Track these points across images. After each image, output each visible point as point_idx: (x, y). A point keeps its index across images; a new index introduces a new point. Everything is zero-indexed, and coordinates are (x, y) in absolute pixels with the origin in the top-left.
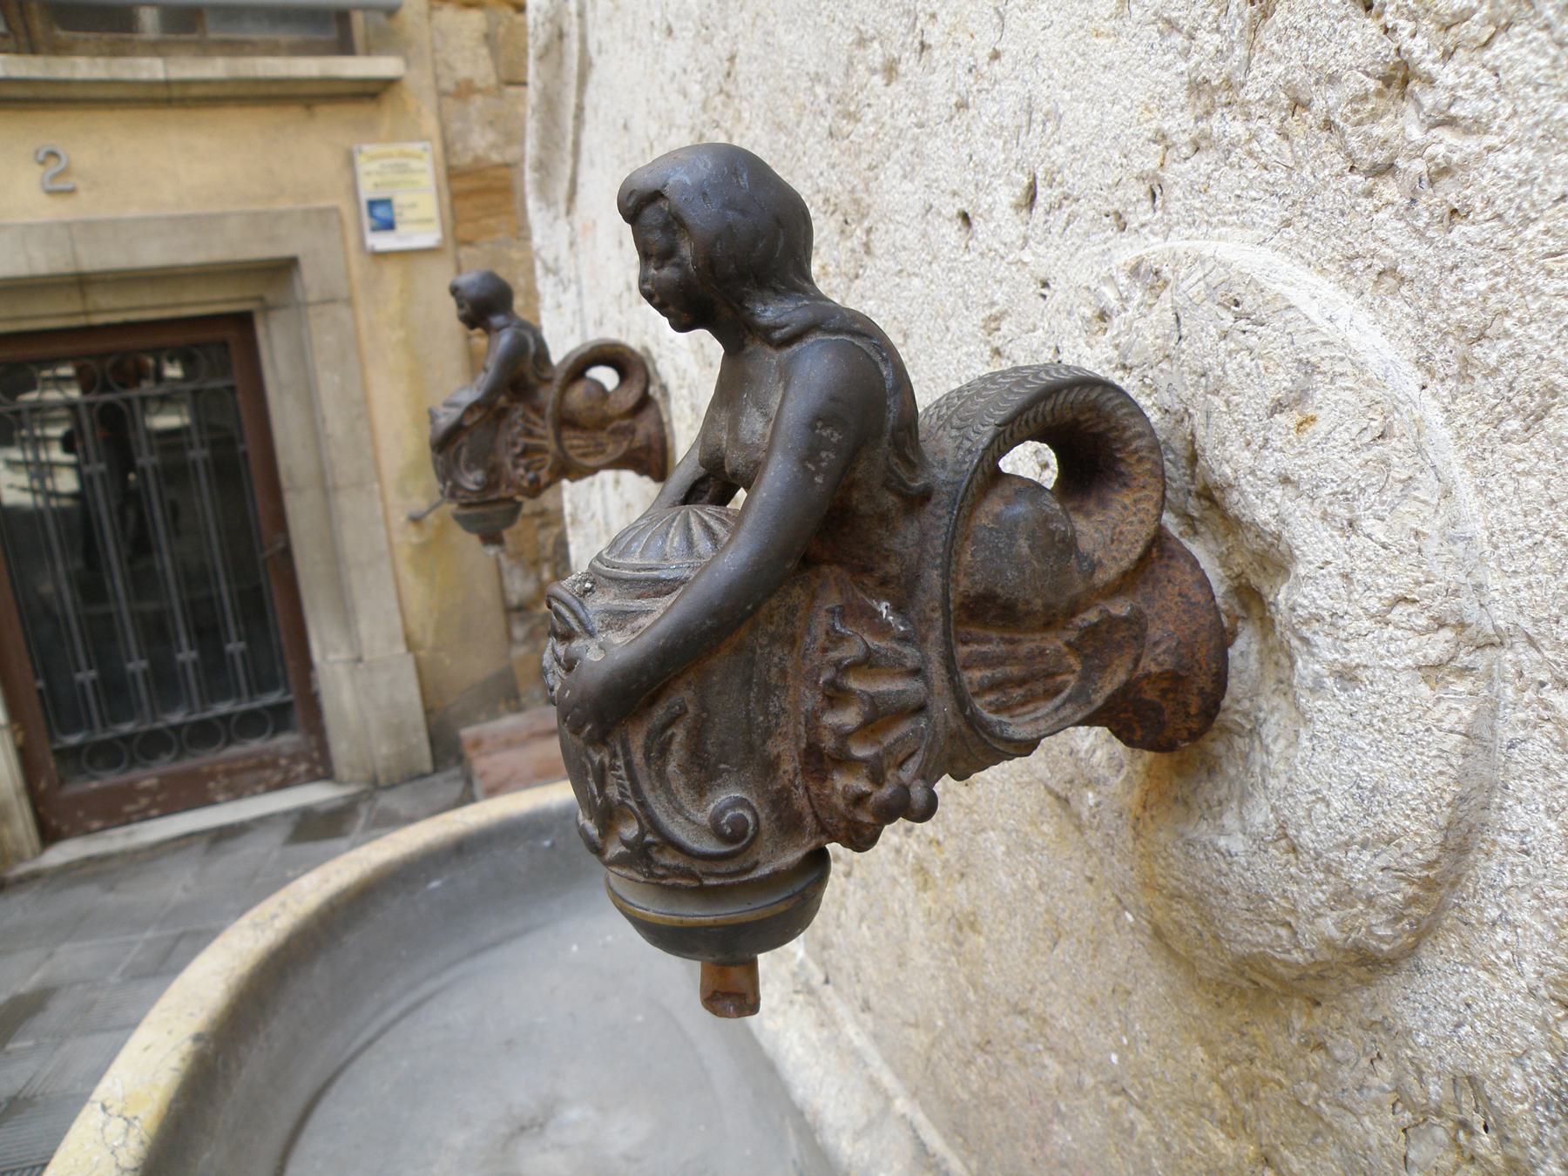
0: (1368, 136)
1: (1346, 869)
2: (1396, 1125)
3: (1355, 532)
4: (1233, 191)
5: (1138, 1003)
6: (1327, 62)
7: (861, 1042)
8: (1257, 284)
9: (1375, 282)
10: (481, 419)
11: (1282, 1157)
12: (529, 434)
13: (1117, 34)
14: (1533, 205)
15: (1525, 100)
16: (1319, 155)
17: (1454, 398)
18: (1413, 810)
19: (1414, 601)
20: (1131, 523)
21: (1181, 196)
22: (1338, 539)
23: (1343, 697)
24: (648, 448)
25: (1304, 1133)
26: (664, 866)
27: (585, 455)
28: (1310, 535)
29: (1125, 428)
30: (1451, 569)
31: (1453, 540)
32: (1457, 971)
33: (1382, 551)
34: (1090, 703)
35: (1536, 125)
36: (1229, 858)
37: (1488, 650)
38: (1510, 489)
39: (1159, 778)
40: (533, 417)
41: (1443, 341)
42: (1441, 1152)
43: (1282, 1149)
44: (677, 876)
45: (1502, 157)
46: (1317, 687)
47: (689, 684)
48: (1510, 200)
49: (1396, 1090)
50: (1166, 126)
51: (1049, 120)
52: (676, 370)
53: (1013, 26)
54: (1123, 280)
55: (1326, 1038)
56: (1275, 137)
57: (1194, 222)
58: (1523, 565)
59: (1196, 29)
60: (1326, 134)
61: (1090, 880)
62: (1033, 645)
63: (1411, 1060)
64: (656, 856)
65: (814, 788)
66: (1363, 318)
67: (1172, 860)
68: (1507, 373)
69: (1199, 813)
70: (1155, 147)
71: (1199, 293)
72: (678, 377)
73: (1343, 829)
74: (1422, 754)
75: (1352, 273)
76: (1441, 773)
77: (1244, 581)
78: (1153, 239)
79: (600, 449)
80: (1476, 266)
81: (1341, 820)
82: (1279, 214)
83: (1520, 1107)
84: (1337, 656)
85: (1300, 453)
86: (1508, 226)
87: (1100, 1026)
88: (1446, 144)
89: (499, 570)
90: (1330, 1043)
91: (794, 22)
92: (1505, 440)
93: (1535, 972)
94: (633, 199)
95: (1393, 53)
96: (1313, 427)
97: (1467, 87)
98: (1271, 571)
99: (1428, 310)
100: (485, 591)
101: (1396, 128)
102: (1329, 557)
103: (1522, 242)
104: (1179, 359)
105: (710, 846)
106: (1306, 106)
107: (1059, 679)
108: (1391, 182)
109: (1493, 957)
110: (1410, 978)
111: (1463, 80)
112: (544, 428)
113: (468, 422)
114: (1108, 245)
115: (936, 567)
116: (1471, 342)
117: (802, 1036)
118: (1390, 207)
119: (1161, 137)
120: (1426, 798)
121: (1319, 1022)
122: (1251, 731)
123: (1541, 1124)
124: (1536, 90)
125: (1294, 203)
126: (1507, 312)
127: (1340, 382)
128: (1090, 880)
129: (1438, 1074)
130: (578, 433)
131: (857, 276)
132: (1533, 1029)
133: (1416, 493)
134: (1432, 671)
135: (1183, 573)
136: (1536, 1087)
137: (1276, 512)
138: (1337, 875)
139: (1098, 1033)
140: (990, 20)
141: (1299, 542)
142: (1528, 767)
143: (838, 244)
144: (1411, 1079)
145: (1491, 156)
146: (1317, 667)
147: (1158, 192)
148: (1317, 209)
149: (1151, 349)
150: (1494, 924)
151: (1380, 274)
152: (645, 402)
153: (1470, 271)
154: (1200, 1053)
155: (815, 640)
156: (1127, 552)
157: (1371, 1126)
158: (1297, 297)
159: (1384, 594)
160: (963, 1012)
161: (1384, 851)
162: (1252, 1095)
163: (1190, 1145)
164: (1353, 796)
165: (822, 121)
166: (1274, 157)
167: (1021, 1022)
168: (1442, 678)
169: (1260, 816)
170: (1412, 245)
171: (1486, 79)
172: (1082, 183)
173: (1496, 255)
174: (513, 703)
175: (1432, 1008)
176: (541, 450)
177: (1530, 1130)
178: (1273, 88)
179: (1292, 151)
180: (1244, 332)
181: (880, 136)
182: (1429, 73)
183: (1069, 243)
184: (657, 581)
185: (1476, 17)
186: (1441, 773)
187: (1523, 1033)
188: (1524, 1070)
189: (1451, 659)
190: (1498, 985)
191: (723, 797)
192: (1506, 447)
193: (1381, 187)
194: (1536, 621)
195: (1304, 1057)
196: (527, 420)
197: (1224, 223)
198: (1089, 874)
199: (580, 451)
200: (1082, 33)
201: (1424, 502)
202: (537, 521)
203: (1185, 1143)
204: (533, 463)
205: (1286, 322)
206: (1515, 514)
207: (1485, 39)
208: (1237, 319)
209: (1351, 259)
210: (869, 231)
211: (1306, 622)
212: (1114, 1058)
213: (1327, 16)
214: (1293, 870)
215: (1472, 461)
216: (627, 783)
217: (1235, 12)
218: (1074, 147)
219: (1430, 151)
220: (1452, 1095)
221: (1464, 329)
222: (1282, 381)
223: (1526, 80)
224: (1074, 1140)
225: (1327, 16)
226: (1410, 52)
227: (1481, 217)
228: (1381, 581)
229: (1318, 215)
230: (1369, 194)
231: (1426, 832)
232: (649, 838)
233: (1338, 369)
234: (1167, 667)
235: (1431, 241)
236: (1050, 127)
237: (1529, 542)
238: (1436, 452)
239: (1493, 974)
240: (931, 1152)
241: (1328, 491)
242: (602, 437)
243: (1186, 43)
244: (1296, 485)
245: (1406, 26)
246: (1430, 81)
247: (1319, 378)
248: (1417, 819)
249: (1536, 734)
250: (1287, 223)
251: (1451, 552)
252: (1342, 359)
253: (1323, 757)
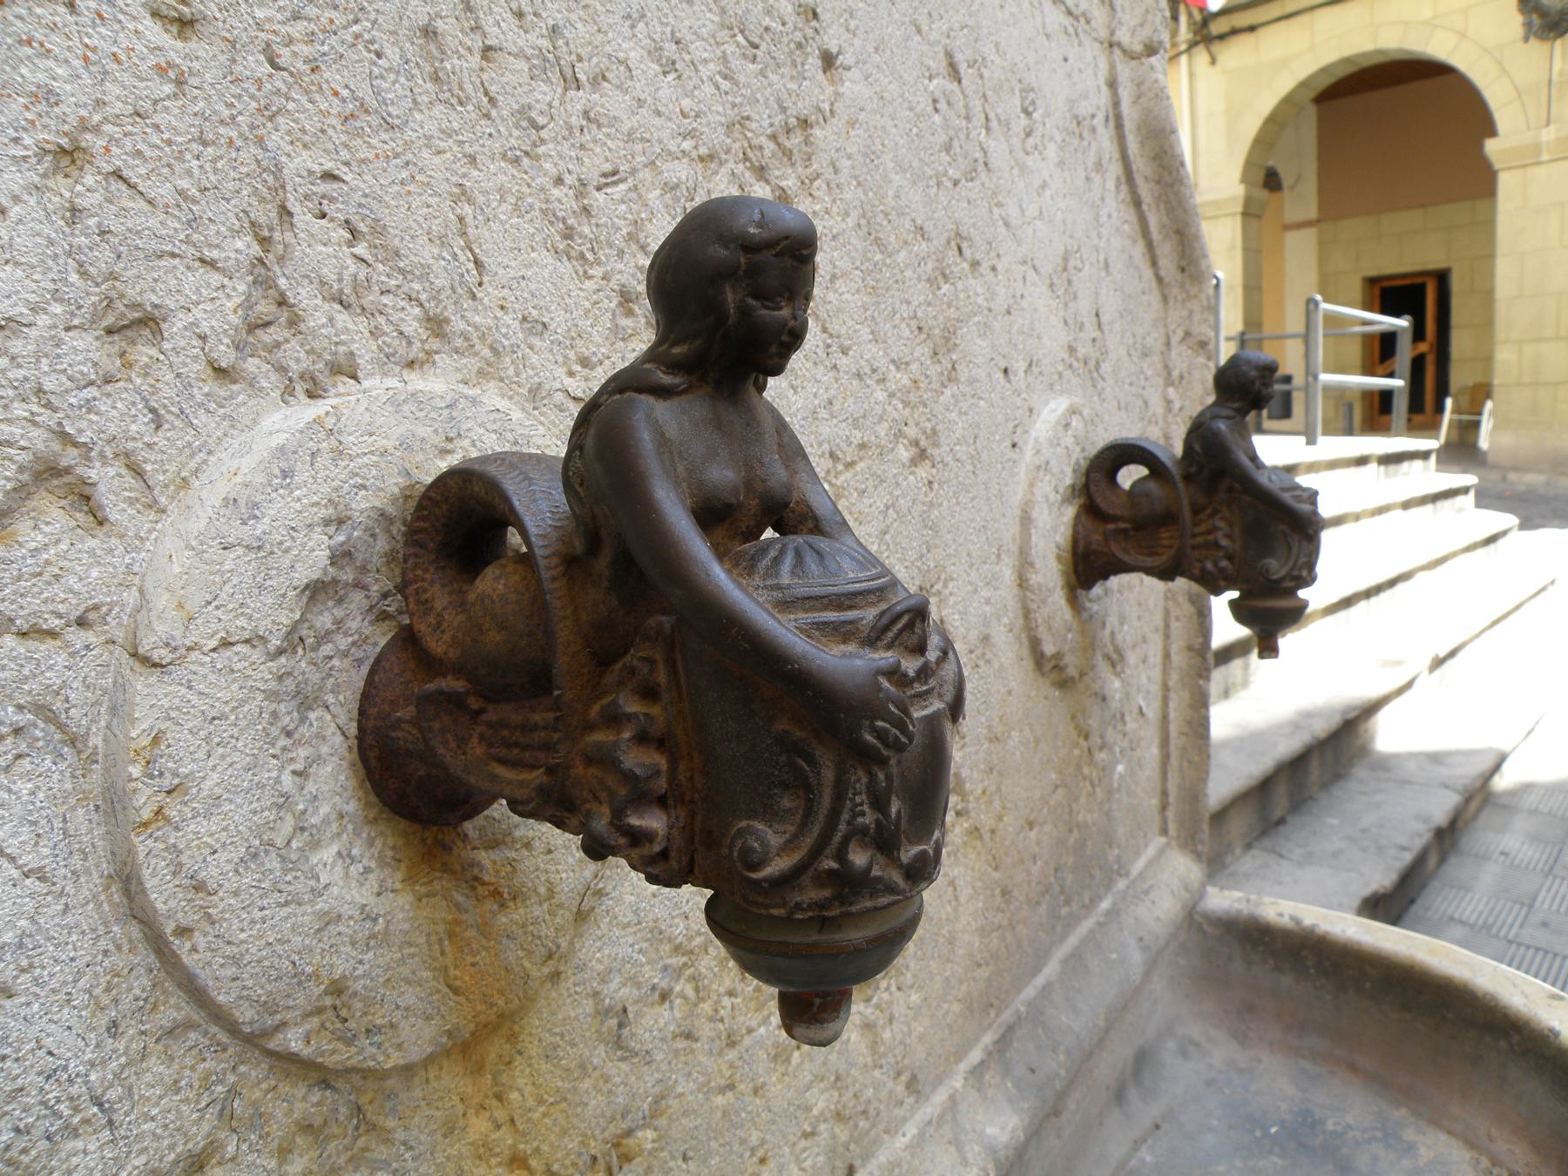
91: (904, 171)
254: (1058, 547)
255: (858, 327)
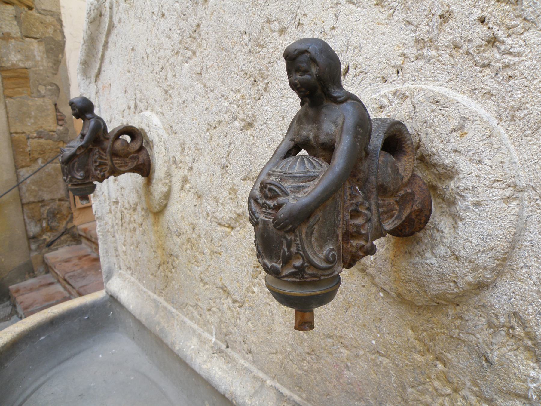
0: (482, 57)
1: (477, 260)
2: (488, 334)
3: (481, 163)
4: (431, 71)
5: (385, 322)
6: (468, 36)
7: (247, 365)
8: (445, 96)
9: (482, 96)
10: (83, 152)
11: (445, 356)
12: (101, 158)
13: (387, 24)
14: (536, 75)
15: (534, 48)
16: (464, 61)
17: (509, 126)
18: (501, 239)
19: (501, 181)
20: (408, 165)
21: (410, 72)
22: (475, 166)
23: (477, 210)
24: (143, 164)
25: (453, 346)
26: (309, 274)
27: (120, 167)
28: (465, 166)
29: (406, 137)
30: (512, 171)
31: (512, 163)
32: (510, 284)
33: (490, 168)
34: (401, 219)
35: (538, 54)
36: (431, 266)
37: (521, 192)
38: (527, 149)
39: (399, 247)
40: (102, 152)
41: (506, 111)
42: (503, 338)
43: (444, 353)
44: (312, 277)
45: (526, 63)
46: (467, 209)
47: (321, 210)
48: (529, 74)
49: (487, 324)
50: (405, 52)
51: (356, 49)
52: (158, 136)
53: (342, 19)
54: (390, 96)
55: (462, 315)
56: (448, 56)
57: (415, 80)
58: (531, 169)
59: (419, 25)
60: (467, 56)
61: (364, 286)
62: (388, 201)
63: (494, 314)
64: (306, 271)
65: (345, 246)
66: (478, 106)
67: (408, 270)
68: (527, 118)
69: (415, 255)
70: (400, 58)
71: (423, 99)
72: (159, 138)
73: (476, 248)
74: (504, 222)
75: (474, 94)
76: (510, 227)
77: (430, 184)
78: (397, 85)
79: (126, 164)
80: (517, 91)
81: (476, 246)
82: (448, 77)
83: (531, 317)
84: (474, 199)
85: (462, 143)
86: (528, 80)
87: (367, 333)
88: (508, 59)
89: (25, 223)
90: (463, 316)
91: (234, 14)
92: (525, 136)
93: (536, 278)
94: (296, 52)
95: (492, 34)
96: (467, 135)
97: (516, 44)
98: (443, 179)
99: (501, 103)
100: (19, 232)
101: (491, 55)
102: (472, 171)
103: (532, 84)
104: (415, 118)
105: (324, 265)
106: (460, 48)
107: (394, 212)
108: (488, 69)
109: (522, 277)
110: (493, 289)
111: (514, 42)
112: (106, 156)
113: (78, 153)
114: (379, 87)
115: (374, 175)
116: (515, 111)
117: (220, 368)
118: (488, 76)
119: (403, 55)
120: (505, 235)
121: (459, 311)
122: (433, 228)
123: (538, 320)
124: (538, 46)
125: (454, 74)
126: (527, 103)
127: (475, 123)
128: (364, 286)
129: (503, 315)
130: (118, 159)
131: (259, 99)
132: (535, 294)
133: (501, 151)
134: (506, 200)
135: (419, 181)
136: (536, 310)
137: (452, 160)
138: (474, 262)
139: (366, 336)
140: (332, 17)
141: (461, 168)
142: (533, 222)
143: (251, 88)
144: (494, 319)
145: (523, 62)
146: (467, 203)
147: (400, 71)
148: (462, 76)
149: (404, 116)
150: (522, 268)
151: (484, 94)
152: (141, 148)
153: (515, 92)
154: (410, 332)
155: (347, 197)
156: (409, 174)
157: (479, 336)
158: (459, 100)
159: (491, 180)
160: (301, 343)
161: (490, 252)
162: (433, 339)
163: (407, 362)
164: (480, 238)
165: (246, 47)
166: (447, 62)
167: (330, 340)
168: (510, 201)
169: (442, 250)
170: (496, 86)
171: (521, 42)
172: (370, 68)
173: (524, 88)
174: (31, 274)
175: (501, 296)
176: (105, 164)
177: (534, 322)
178: (448, 42)
179: (454, 60)
180: (440, 110)
181: (276, 52)
182: (503, 40)
183: (362, 86)
184: (308, 177)
185: (519, 26)
186: (510, 227)
187: (532, 297)
188: (532, 306)
189: (513, 195)
190: (523, 285)
191: (328, 248)
192: (526, 138)
193: (485, 70)
194: (535, 183)
195: (453, 322)
196: (100, 153)
197: (427, 80)
198: (363, 284)
199: (119, 165)
200: (372, 23)
201: (504, 154)
202: (40, 204)
203: (404, 362)
204: (103, 169)
205: (456, 107)
206: (529, 155)
207: (522, 32)
208: (437, 106)
209: (474, 90)
210: (267, 84)
211: (463, 191)
212: (374, 342)
213: (469, 24)
214: (457, 264)
215: (515, 142)
216: (300, 246)
217: (435, 20)
218: (367, 57)
219: (503, 61)
220: (508, 320)
221: (513, 108)
222: (455, 123)
223: (535, 43)
224: (354, 374)
225: (469, 24)
226: (497, 34)
227: (519, 78)
228: (490, 176)
229: (463, 78)
230: (481, 72)
231: (505, 244)
232: (306, 264)
233: (475, 119)
234: (419, 208)
235: (503, 84)
236: (356, 51)
237: (534, 162)
238: (505, 141)
239: (522, 282)
240: (285, 395)
241: (471, 153)
242: (127, 160)
243: (415, 28)
244: (460, 152)
245: (496, 28)
246: (503, 42)
247: (468, 122)
248: (502, 241)
249: (535, 213)
250: (451, 80)
251: (512, 166)
252: (476, 116)
253: (469, 229)
254: (90, 231)
255: (216, 82)
